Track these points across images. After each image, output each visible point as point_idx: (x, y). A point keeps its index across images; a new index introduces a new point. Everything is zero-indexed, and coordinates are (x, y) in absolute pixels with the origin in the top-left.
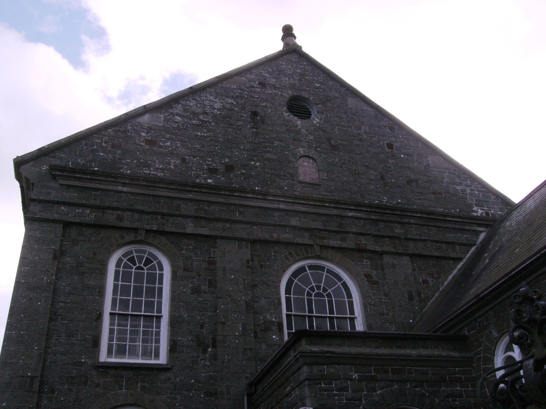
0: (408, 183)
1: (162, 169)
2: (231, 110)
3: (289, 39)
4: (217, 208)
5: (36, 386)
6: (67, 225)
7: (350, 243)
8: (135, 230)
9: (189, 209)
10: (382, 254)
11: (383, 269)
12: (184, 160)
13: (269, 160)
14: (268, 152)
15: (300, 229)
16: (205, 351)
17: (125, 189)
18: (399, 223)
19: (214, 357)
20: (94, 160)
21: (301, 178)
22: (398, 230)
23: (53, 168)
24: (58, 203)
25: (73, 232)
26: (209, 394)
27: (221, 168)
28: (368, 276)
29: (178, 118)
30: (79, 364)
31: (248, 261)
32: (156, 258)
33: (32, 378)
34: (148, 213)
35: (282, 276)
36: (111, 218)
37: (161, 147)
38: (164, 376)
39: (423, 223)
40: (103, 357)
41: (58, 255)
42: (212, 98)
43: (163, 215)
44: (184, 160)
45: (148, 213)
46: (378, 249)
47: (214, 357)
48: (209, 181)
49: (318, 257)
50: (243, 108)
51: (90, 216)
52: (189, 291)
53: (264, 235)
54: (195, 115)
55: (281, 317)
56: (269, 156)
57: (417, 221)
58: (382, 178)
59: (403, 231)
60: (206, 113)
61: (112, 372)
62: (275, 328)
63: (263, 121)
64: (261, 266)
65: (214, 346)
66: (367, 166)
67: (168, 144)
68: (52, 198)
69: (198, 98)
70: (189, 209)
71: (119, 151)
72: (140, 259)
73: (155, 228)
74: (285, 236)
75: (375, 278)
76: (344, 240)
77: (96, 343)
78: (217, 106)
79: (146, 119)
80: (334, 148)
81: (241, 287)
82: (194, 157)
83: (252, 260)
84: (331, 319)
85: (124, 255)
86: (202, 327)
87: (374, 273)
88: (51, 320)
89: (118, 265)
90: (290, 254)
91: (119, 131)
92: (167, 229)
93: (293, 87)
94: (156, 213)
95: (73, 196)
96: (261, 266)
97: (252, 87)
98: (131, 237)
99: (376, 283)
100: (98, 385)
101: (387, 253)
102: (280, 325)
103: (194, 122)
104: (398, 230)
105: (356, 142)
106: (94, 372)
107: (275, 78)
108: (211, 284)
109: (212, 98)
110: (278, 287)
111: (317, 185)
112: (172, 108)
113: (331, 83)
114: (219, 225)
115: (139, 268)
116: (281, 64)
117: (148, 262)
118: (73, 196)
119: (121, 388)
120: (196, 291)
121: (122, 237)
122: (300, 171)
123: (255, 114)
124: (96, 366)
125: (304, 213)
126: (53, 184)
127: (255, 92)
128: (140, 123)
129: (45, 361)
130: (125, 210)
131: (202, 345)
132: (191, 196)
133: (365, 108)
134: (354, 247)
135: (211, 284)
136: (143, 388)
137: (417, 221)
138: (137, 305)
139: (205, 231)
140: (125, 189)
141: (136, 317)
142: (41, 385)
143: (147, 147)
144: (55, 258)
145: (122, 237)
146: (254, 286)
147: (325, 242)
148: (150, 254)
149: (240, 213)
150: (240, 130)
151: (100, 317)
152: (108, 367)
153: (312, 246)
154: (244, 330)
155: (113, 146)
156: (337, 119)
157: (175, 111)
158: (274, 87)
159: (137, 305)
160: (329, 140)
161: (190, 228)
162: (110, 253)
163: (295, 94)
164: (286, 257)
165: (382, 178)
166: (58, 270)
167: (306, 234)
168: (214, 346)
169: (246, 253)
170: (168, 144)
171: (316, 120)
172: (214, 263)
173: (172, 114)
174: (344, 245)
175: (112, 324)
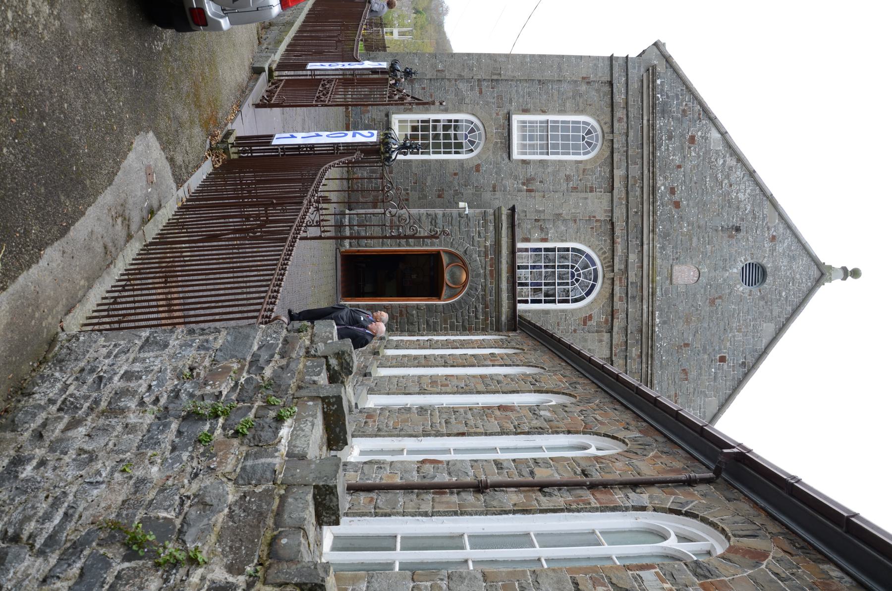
0: (684, 370)
1: (668, 149)
2: (738, 208)
3: (841, 273)
4: (638, 193)
5: (495, 77)
6: (611, 84)
7: (618, 305)
8: (612, 132)
9: (634, 171)
10: (611, 331)
11: (597, 332)
12: (679, 167)
13: (691, 240)
14: (699, 239)
15: (627, 261)
16: (523, 184)
17: (645, 122)
18: (641, 352)
19: (520, 191)
20: (668, 97)
21: (676, 268)
22: (634, 352)
23: (654, 67)
24: (627, 75)
25: (607, 88)
26: (494, 187)
27: (676, 198)
28: (590, 317)
29: (721, 162)
30: (511, 101)
31: (594, 217)
32: (593, 150)
33: (500, 74)
34: (627, 140)
35: (585, 244)
36: (620, 113)
37: (690, 148)
38: (505, 156)
39: (644, 376)
40: (516, 119)
41: (587, 81)
42: (748, 191)
43: (627, 151)
44: (679, 167)
45: (627, 140)
46: (615, 329)
47: (520, 191)
48: (663, 188)
49: (604, 277)
50: (742, 220)
51: (619, 98)
52: (568, 173)
53: (618, 232)
54: (728, 177)
55: (552, 241)
56: (695, 240)
57: (644, 370)
58: (687, 345)
59: (634, 355)
60: (731, 186)
61: (507, 123)
62: (543, 236)
63: (731, 237)
64: (592, 228)
65: (528, 191)
66: (696, 332)
67: (693, 154)
68: (630, 71)
69: (746, 178)
70: (634, 171)
71: (679, 115)
72: (475, 137)
73: (615, 146)
74: (619, 249)
75: (589, 323)
76: (621, 299)
77: (526, 111)
78: (741, 196)
79: (715, 135)
80: (712, 302)
81: (573, 211)
82: (684, 176)
83: (597, 221)
84: (554, 284)
85: (592, 127)
86: (541, 182)
87: (593, 323)
88: (539, 81)
89: (584, 123)
90: (605, 253)
91: (699, 114)
92: (615, 155)
93: (777, 269)
94: (627, 146)
95: (634, 85)
96: (592, 228)
97: (768, 229)
98: (607, 129)
99: (585, 324)
100: (497, 114)
101: (611, 336)
102: (545, 240)
103: (720, 175)
104: (634, 352)
105: (722, 324)
106: (506, 111)
107: (784, 252)
108: (575, 189)
109: (748, 191)
110: (576, 240)
111: (671, 280)
112: (731, 156)
113: (789, 309)
114: (624, 195)
115: (584, 138)
116: (802, 260)
117: (589, 144)
118: (634, 85)
119: (497, 129)
120: (568, 178)
121: (605, 123)
122: (684, 267)
123: (738, 229)
124: (509, 113)
125: (642, 267)
126: (643, 70)
127: (762, 231)
128: (710, 130)
129: (512, 80)
130: (627, 123)
131: (528, 181)
132: (646, 172)
133: (764, 341)
134: (615, 308)
135: (575, 189)
136: (497, 143)
137: (644, 370)
138: (555, 138)
139: (617, 184)
140: (645, 122)
141: (546, 137)
142: (497, 80)
143: (688, 137)
144: (583, 78)
145: (605, 123)
146: (575, 221)
147: (617, 282)
148: (596, 145)
149: (636, 212)
150: (718, 215)
151: (544, 112)
152: (509, 119)
153: (613, 271)
154: (540, 212)
155: (684, 111)
156: (745, 310)
157: (728, 159)
158: (773, 250)
159: (555, 138)
160: (720, 297)
161: (619, 173)
162: (592, 115)
163: (768, 270)
164: (602, 249)
165: (687, 345)
166: (576, 82)
167: (623, 267)
168: (528, 191)
169: (602, 216)
170: (693, 154)
171: (741, 288)
172: (591, 191)
173: (724, 157)
174: (616, 299)
175: (541, 122)
